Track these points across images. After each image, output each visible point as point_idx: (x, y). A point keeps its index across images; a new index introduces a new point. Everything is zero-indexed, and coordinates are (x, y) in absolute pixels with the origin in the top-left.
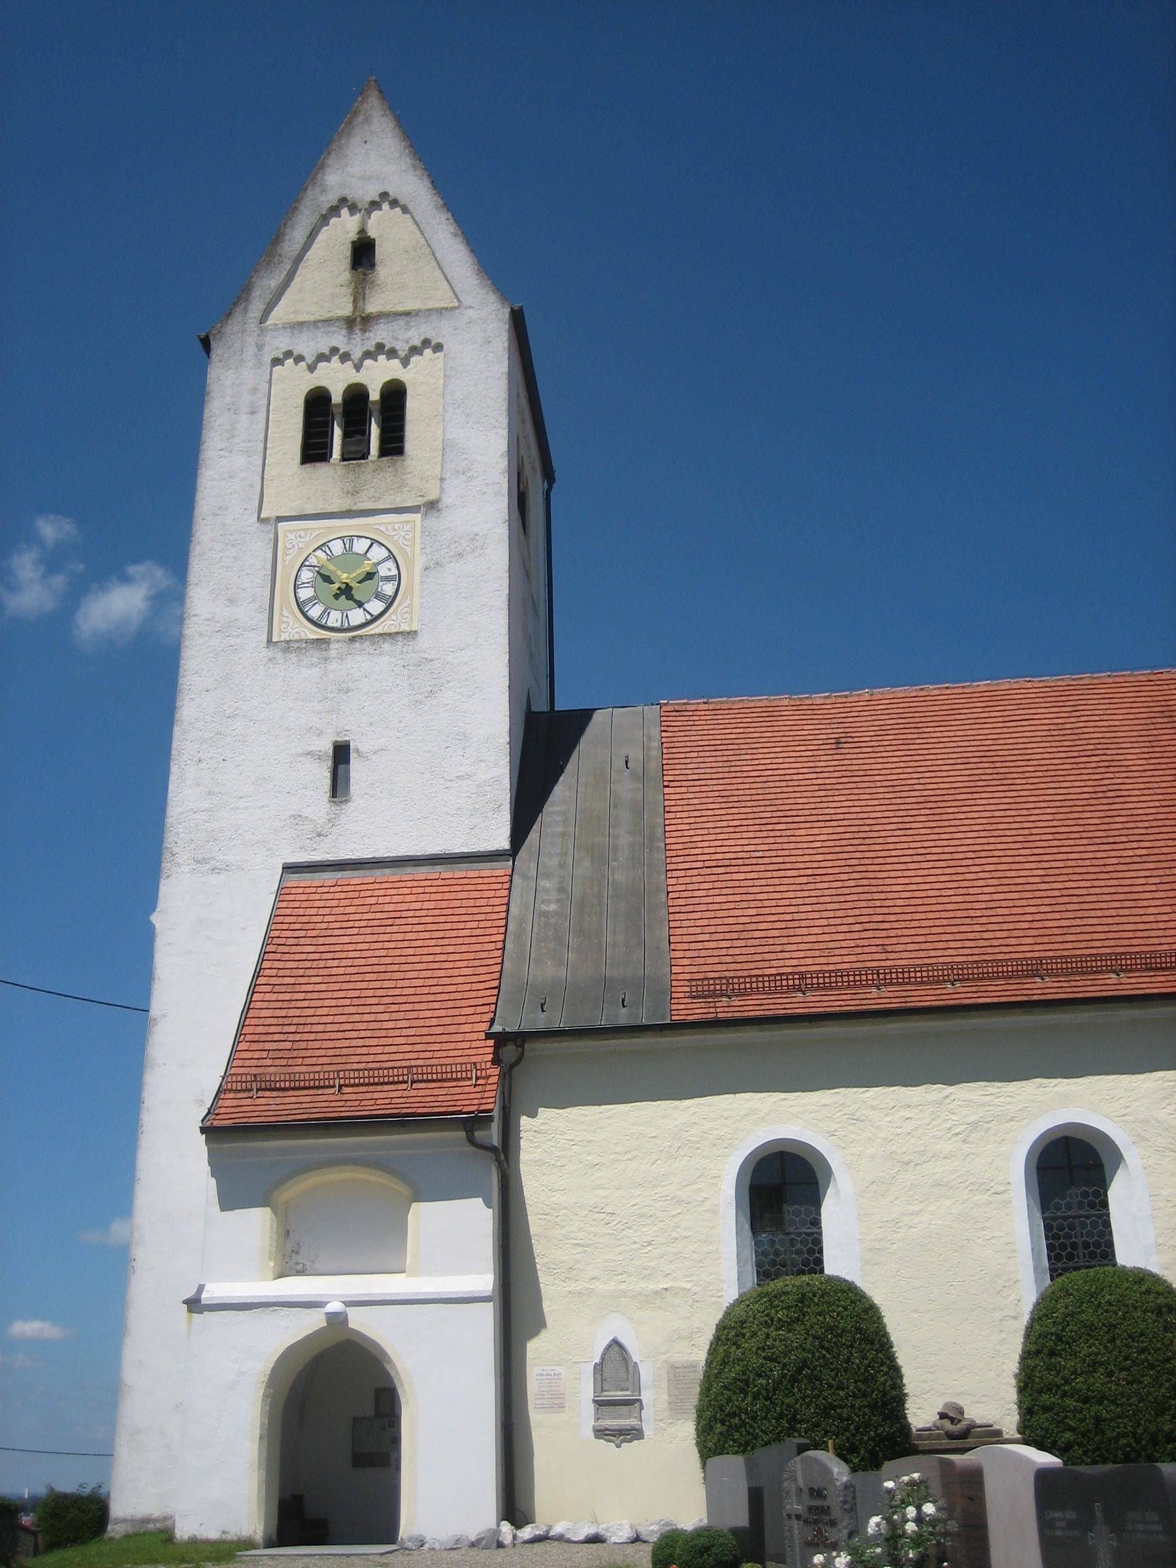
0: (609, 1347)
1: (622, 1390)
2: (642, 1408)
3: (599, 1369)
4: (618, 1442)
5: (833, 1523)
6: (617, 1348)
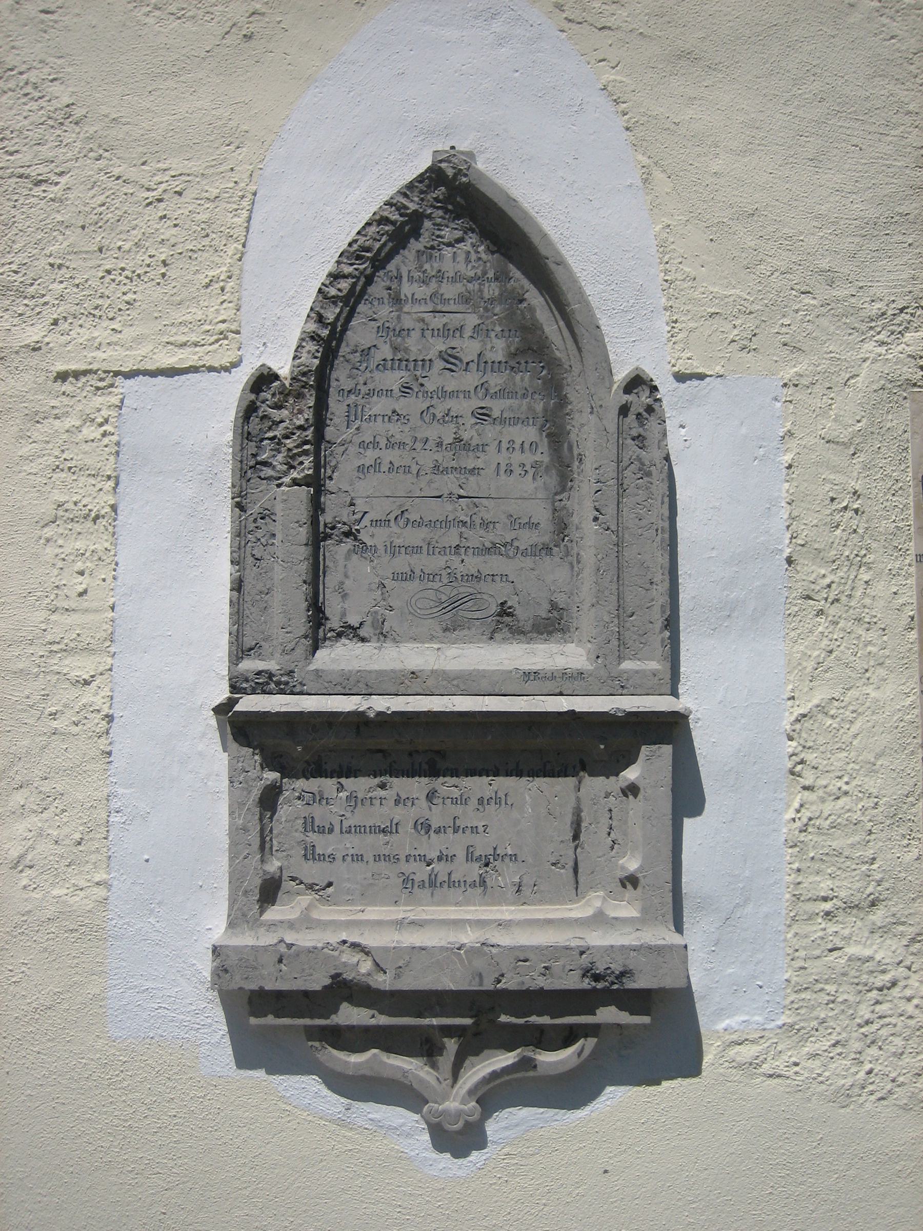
0: (393, 236)
1: (505, 622)
2: (687, 796)
3: (291, 427)
4: (456, 1102)
5: (874, 924)
6: (462, 257)
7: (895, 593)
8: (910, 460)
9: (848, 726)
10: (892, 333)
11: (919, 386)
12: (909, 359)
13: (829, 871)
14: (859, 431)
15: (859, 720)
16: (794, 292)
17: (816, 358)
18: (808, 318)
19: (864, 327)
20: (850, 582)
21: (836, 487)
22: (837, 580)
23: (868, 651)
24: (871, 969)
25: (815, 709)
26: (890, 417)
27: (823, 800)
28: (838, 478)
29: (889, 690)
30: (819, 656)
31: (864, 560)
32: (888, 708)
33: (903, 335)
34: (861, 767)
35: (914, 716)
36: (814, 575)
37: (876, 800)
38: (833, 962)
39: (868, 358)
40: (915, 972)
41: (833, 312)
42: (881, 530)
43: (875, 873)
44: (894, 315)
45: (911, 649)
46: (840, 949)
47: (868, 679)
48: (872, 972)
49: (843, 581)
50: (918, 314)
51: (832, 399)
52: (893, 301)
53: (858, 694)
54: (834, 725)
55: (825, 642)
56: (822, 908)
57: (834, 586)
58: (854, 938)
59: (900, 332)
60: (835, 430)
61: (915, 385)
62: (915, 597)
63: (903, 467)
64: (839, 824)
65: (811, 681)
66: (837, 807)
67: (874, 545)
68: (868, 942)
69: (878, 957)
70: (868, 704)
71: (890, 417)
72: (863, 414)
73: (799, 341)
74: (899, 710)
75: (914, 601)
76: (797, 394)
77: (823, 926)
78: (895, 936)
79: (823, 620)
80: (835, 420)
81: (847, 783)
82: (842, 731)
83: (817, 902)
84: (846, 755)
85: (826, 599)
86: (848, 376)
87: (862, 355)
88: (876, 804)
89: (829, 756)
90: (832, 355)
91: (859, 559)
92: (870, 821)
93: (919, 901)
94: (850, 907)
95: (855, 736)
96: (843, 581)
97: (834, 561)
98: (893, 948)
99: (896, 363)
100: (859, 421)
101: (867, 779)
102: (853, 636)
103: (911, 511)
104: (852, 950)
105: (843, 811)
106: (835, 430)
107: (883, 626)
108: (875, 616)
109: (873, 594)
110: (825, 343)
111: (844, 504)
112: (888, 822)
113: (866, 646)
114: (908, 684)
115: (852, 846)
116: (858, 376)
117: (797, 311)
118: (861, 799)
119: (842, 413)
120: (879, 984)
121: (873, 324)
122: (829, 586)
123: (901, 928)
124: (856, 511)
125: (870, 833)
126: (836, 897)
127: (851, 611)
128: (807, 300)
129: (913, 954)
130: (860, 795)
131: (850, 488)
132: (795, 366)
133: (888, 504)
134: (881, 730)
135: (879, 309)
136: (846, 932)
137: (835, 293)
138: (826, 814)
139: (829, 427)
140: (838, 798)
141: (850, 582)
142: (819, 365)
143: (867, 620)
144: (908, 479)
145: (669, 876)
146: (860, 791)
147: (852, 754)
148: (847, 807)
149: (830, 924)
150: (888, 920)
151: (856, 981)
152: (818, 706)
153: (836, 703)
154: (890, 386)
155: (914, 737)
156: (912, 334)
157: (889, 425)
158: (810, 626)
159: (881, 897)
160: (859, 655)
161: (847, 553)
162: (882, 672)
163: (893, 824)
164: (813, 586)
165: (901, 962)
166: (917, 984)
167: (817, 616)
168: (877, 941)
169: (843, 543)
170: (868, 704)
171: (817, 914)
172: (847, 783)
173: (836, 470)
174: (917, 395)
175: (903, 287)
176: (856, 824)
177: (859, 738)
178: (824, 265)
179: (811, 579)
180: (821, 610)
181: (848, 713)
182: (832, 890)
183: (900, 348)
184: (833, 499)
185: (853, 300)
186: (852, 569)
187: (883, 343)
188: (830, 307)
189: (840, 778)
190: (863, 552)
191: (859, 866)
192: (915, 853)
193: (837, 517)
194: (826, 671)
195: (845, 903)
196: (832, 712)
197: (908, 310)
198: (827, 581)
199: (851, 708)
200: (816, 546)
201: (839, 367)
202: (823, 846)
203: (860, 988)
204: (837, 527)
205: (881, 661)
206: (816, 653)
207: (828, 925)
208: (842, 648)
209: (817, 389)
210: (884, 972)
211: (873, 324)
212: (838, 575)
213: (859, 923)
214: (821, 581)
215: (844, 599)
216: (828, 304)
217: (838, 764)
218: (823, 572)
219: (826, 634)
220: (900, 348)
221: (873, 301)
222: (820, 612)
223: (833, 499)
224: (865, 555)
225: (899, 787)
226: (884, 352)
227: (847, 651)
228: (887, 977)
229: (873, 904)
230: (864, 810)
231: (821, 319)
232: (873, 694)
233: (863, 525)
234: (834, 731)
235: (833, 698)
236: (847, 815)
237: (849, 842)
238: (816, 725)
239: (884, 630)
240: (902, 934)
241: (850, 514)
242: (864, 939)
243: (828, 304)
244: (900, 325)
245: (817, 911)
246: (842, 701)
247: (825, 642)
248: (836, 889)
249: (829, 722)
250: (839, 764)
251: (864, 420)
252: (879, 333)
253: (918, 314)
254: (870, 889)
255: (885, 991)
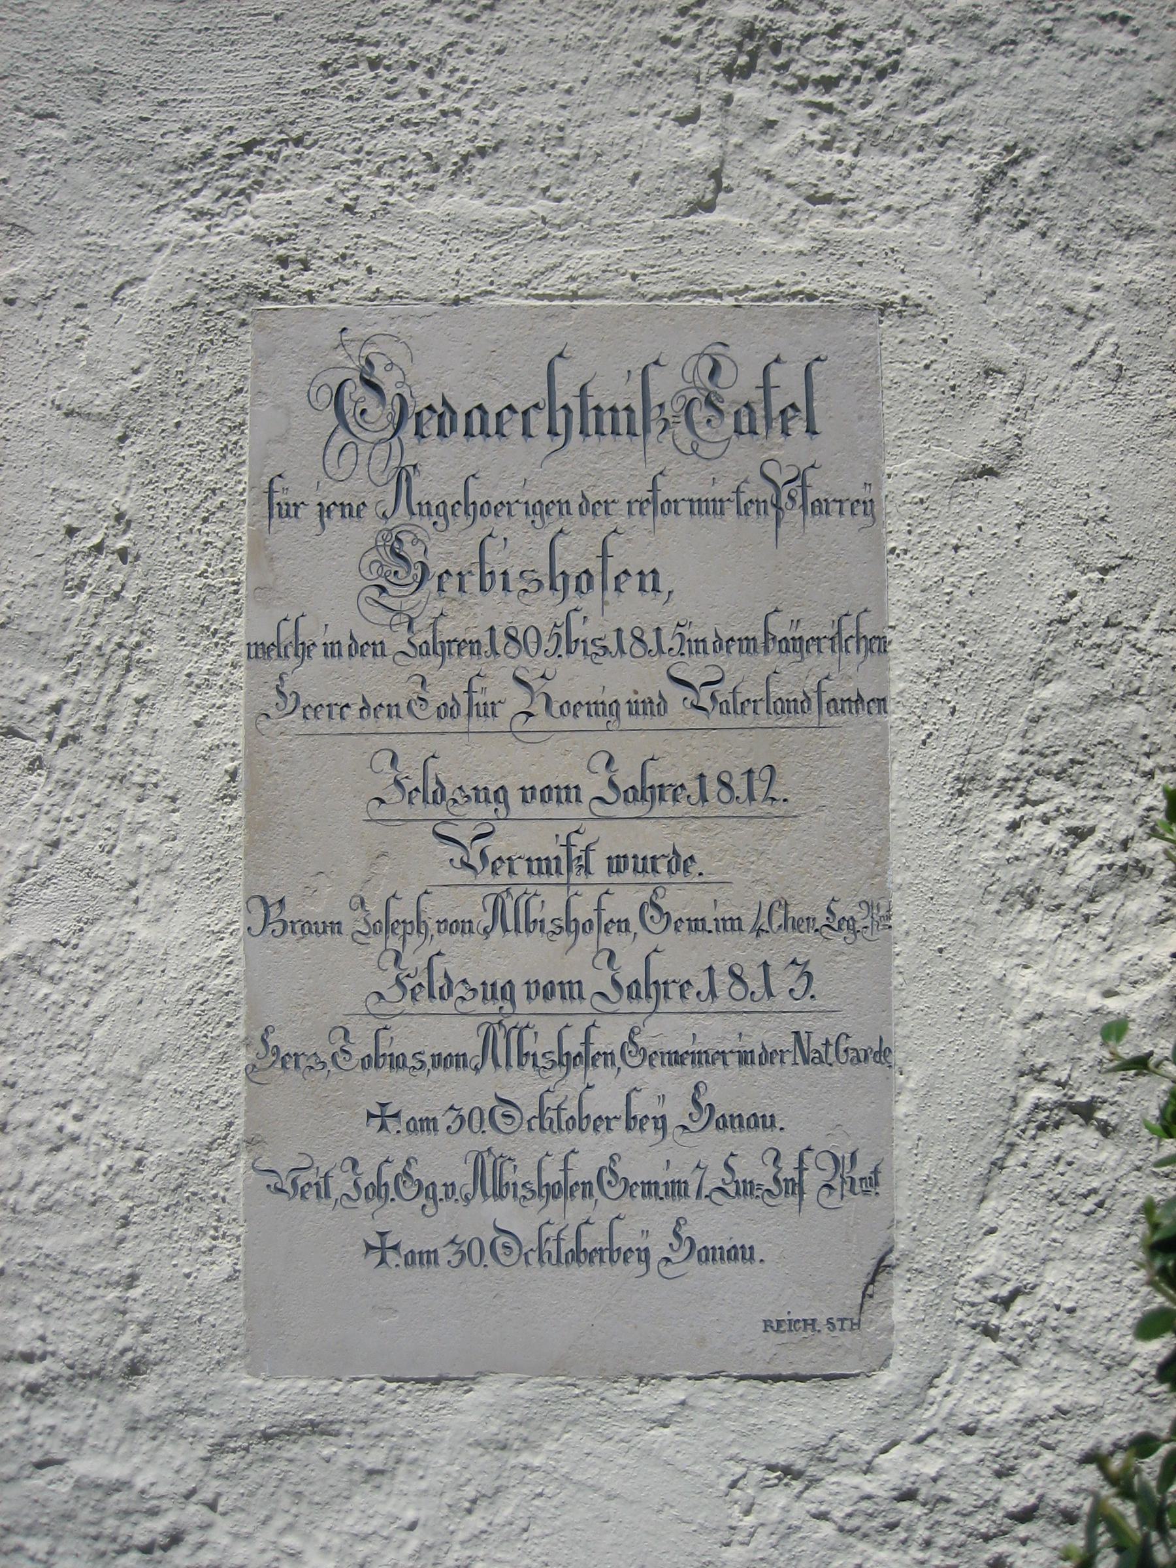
5: (135, 1411)
7: (198, 724)
8: (247, 449)
9: (84, 999)
10: (225, 194)
11: (276, 299)
12: (257, 244)
13: (37, 1300)
14: (136, 390)
15: (111, 986)
16: (21, 116)
17: (57, 245)
18: (46, 165)
19: (162, 183)
20: (103, 701)
21: (80, 506)
22: (74, 696)
23: (137, 843)
24: (124, 1506)
25: (12, 963)
26: (206, 362)
27: (25, 1153)
28: (87, 488)
29: (178, 925)
30: (28, 853)
31: (137, 655)
32: (172, 962)
33: (249, 198)
34: (110, 1085)
35: (229, 980)
36: (24, 687)
37: (138, 1154)
38: (43, 1489)
39: (165, 244)
40: (224, 1514)
41: (98, 152)
42: (173, 592)
43: (136, 1306)
44: (230, 156)
45: (228, 840)
46: (60, 1462)
47: (136, 901)
48: (127, 1513)
49: (87, 698)
50: (284, 154)
51: (84, 327)
52: (231, 129)
53: (110, 932)
54: (54, 997)
55: (44, 824)
56: (21, 1376)
57: (67, 709)
58: (91, 1441)
59: (241, 192)
60: (85, 390)
61: (265, 296)
62: (241, 732)
63: (231, 460)
64: (58, 1203)
65: (9, 905)
66: (54, 1168)
67: (158, 625)
68: (123, 1450)
69: (140, 1482)
70: (130, 954)
71: (206, 362)
72: (146, 355)
73: (24, 213)
74: (197, 968)
75: (240, 740)
76: (12, 320)
77: (22, 1413)
78: (182, 1437)
79: (42, 779)
80: (87, 370)
81: (77, 1118)
82: (71, 1008)
83: (12, 1364)
84: (77, 1057)
85: (50, 736)
86: (120, 280)
87: (155, 239)
88: (139, 1162)
89: (40, 1061)
90: (89, 239)
91: (125, 652)
92: (125, 1197)
93: (232, 1366)
94: (83, 1376)
95: (100, 1020)
96: (87, 698)
97: (70, 658)
98: (177, 1463)
99: (225, 253)
100: (136, 371)
101: (119, 1111)
102: (106, 812)
103: (243, 554)
104: (85, 1466)
105: (68, 1176)
106: (85, 390)
107: (170, 792)
108: (157, 771)
109: (152, 725)
110: (77, 216)
111: (96, 540)
112: (165, 1201)
113: (134, 832)
114: (221, 913)
115: (86, 1248)
116: (143, 280)
117: (23, 153)
118: (108, 1153)
119: (101, 355)
120: (141, 1539)
121: (184, 176)
122: (56, 709)
123: (194, 1422)
124: (123, 554)
125: (126, 1222)
126: (53, 1354)
127: (105, 761)
128: (47, 130)
129: (219, 1476)
130: (104, 1143)
131: (110, 508)
132: (11, 263)
133: (192, 539)
134: (156, 1008)
135: (198, 145)
136: (73, 1428)
137: (106, 114)
138: (29, 1181)
139: (73, 385)
140: (58, 1148)
141: (103, 701)
142: (62, 259)
143: (137, 779)
144: (240, 488)
145: (772, 979)
146: (106, 1136)
147: (91, 1056)
148: (76, 1168)
149: (39, 1410)
150: (165, 1404)
151: (92, 1531)
152: (18, 957)
153: (61, 952)
154: (208, 299)
155: (229, 1025)
156: (271, 195)
157: (202, 377)
158: (14, 791)
159: (152, 1357)
160: (117, 851)
161: (96, 642)
162: (164, 887)
163: (177, 1204)
164: (20, 710)
165: (193, 1492)
166: (225, 1540)
167: (31, 770)
168: (145, 1448)
169: (91, 620)
170: (130, 954)
171: (12, 1389)
172: (77, 1118)
173: (81, 470)
174: (272, 316)
175: (255, 101)
176: (93, 1204)
177: (107, 1024)
178: (86, 58)
179: (18, 694)
180: (39, 758)
181: (86, 971)
182: (42, 1338)
183: (239, 223)
184: (71, 531)
185: (143, 128)
186: (108, 674)
187: (199, 214)
188: (93, 144)
189: (64, 1106)
190: (135, 638)
191: (101, 1291)
192: (225, 1265)
193: (80, 567)
194: (43, 885)
195: (71, 1367)
196: (50, 971)
197: (263, 148)
198: (52, 698)
199: (93, 961)
200: (31, 626)
201: (103, 263)
202: (24, 1248)
203: (101, 1545)
204: (80, 587)
205: (165, 864)
206: (24, 847)
207: (35, 1413)
208: (80, 836)
209: (57, 309)
210: (154, 1513)
211: (184, 176)
212: (77, 686)
213: (104, 1410)
214: (39, 698)
215: (88, 735)
216: (90, 138)
217: (59, 1078)
218: (44, 679)
219: (46, 808)
220: (239, 223)
221: (187, 130)
222: (36, 764)
223: (71, 531)
224: (138, 645)
225: (189, 1128)
226: (202, 231)
227: (90, 844)
228: (160, 1525)
229: (134, 1369)
230: (112, 1174)
231: (73, 168)
232: (143, 934)
233: (136, 584)
234: (53, 1009)
235: (55, 941)
236: (75, 1184)
237: (80, 1240)
238: (15, 996)
239: (173, 799)
240: (196, 1435)
241: (105, 561)
242: (112, 1444)
243: (90, 138)
244: (242, 177)
245: (10, 1382)
246: (76, 946)
247: (44, 824)
248: (50, 1338)
249: (45, 989)
250: (62, 1078)
251: (148, 370)
252: (195, 194)
253: (284, 154)
254: (125, 1340)
255: (158, 1554)
